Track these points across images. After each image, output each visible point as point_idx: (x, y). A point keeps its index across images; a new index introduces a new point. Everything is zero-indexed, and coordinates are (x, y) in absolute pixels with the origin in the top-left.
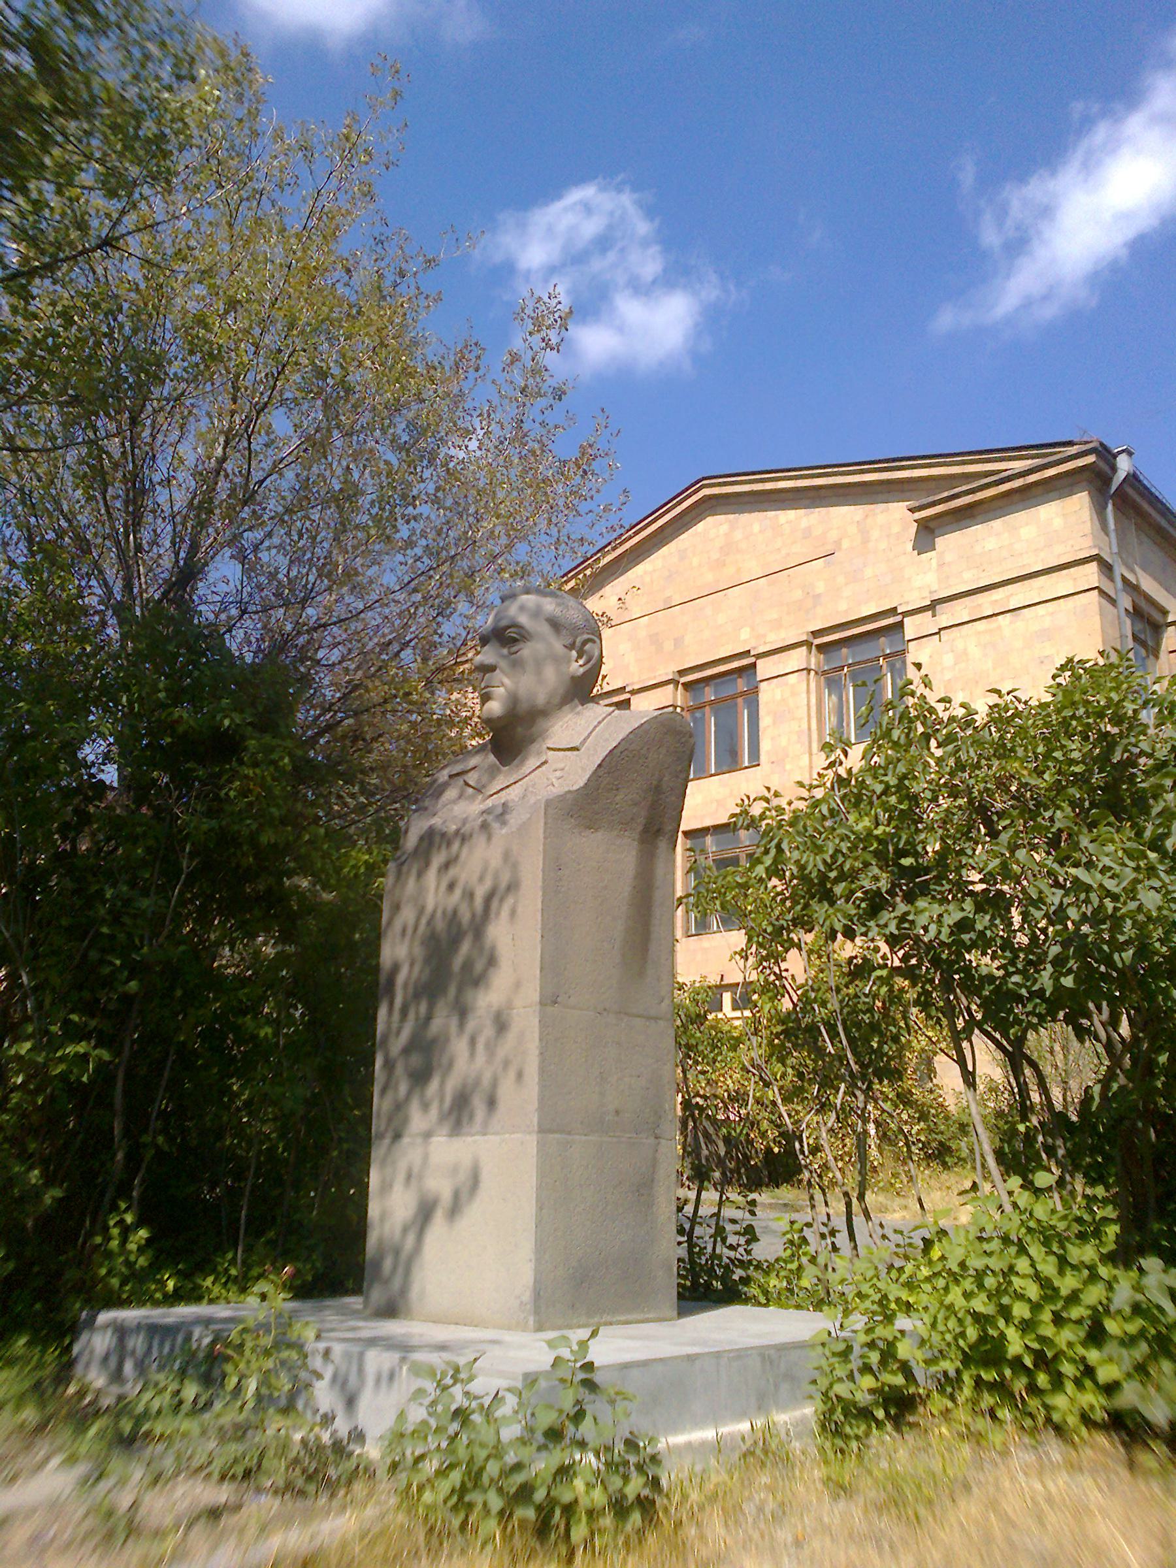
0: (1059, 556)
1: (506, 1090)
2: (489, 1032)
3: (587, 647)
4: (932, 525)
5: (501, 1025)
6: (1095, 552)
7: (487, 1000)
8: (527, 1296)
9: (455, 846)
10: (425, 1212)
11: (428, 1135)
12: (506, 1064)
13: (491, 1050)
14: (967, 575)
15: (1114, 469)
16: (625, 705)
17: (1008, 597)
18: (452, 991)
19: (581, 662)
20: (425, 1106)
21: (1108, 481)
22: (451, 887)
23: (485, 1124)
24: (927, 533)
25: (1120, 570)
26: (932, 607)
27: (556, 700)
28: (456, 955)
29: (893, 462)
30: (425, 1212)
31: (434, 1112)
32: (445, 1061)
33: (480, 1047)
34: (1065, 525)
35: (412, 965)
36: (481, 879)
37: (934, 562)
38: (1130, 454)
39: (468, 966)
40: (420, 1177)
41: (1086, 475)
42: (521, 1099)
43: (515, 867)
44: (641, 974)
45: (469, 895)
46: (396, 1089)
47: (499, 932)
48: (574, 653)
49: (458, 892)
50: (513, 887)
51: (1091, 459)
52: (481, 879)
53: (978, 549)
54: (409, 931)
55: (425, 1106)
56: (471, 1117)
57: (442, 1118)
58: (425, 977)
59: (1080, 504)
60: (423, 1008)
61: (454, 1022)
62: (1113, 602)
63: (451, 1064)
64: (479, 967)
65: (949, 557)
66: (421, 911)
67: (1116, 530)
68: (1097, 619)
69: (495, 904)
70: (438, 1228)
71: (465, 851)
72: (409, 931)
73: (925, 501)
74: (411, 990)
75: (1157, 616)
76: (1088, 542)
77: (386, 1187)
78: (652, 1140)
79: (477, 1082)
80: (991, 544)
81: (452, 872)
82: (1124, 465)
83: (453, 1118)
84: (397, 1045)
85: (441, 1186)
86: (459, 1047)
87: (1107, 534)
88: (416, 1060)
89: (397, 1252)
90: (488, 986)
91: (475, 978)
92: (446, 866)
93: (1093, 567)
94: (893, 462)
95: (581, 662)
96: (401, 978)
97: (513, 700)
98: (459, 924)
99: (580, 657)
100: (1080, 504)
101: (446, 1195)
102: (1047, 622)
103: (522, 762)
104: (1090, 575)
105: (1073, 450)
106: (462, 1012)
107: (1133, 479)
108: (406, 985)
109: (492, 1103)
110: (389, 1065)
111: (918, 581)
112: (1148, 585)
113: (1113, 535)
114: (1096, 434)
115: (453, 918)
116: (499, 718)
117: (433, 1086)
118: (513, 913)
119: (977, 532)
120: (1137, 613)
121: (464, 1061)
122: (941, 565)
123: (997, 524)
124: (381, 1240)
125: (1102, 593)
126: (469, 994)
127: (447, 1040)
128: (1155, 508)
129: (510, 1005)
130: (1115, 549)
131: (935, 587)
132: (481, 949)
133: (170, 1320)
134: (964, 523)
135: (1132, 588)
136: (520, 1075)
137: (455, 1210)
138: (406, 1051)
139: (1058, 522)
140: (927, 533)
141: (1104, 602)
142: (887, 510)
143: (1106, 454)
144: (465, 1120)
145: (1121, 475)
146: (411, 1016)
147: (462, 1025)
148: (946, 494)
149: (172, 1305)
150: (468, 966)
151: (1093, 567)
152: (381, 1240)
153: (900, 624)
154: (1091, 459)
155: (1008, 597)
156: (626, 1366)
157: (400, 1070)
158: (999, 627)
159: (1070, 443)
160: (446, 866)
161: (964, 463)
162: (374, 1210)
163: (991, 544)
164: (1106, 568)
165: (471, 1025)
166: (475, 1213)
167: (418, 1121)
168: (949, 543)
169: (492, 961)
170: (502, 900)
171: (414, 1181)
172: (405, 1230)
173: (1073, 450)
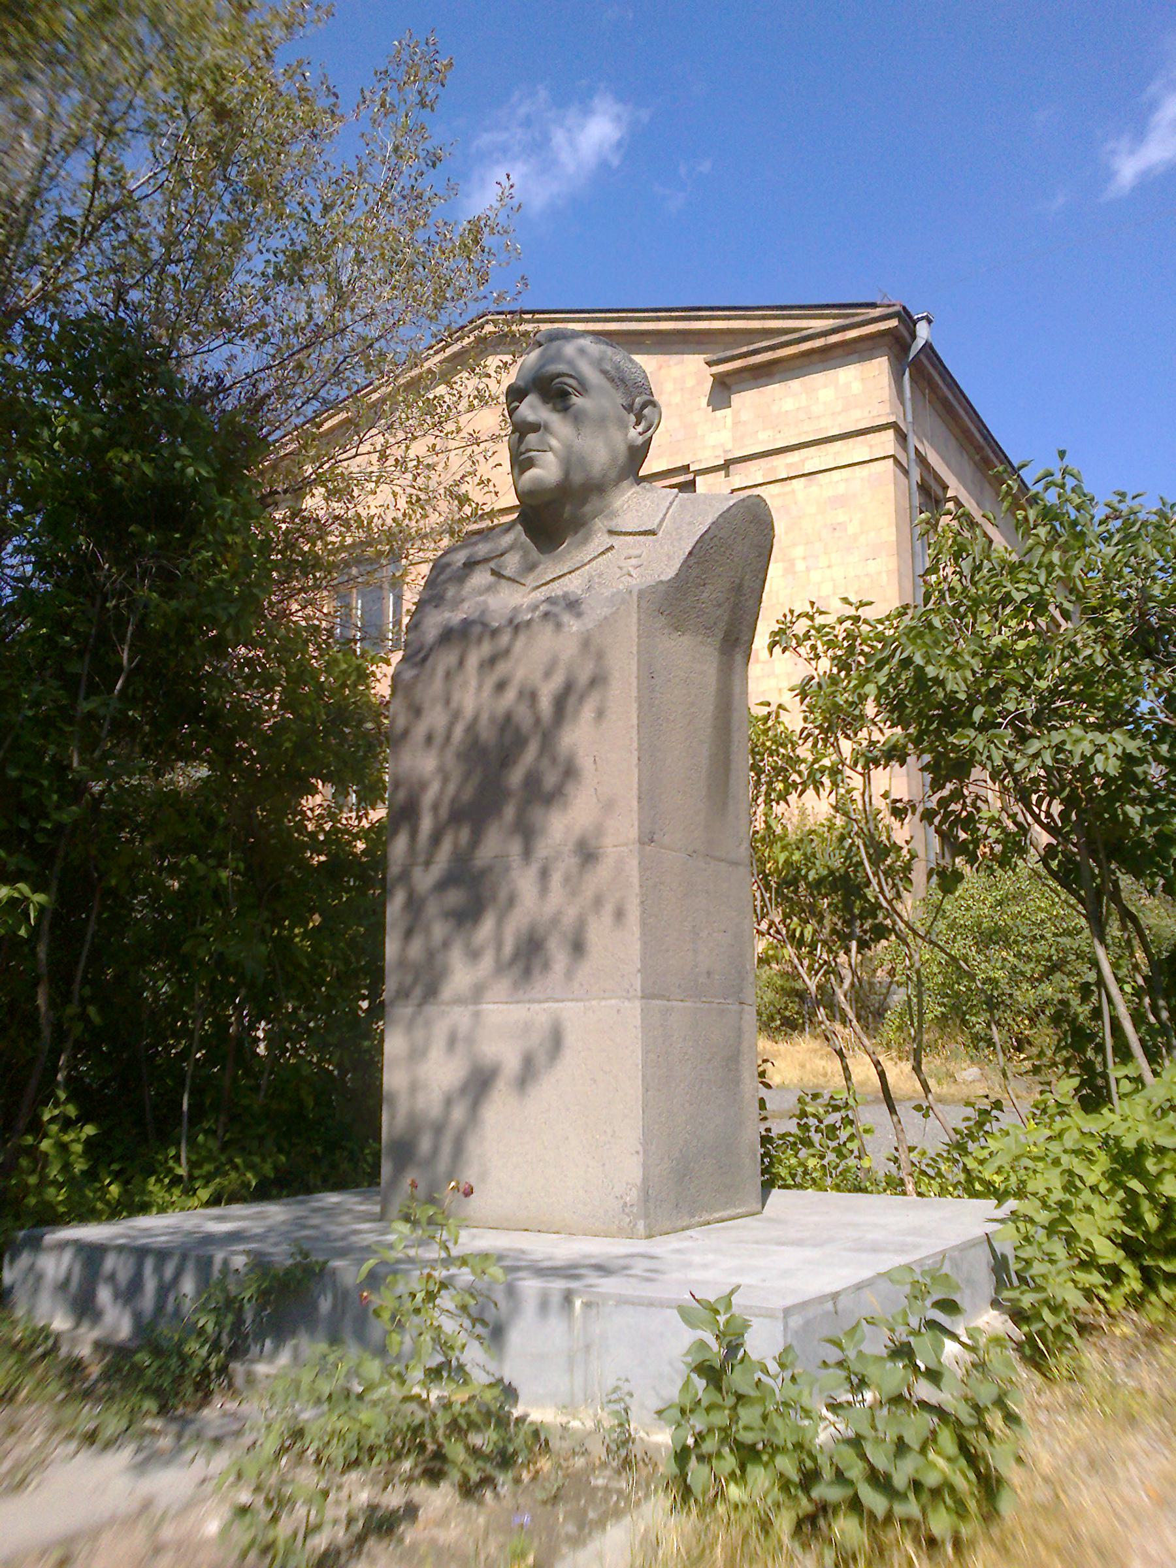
0: (857, 420)
1: (599, 932)
2: (568, 862)
3: (646, 411)
4: (727, 380)
5: (587, 853)
6: (892, 419)
7: (561, 827)
8: (633, 1196)
9: (505, 639)
10: (480, 1083)
11: (477, 993)
12: (598, 902)
13: (572, 885)
14: (762, 436)
15: (914, 336)
16: (690, 486)
17: (803, 461)
18: (509, 812)
19: (640, 429)
20: (474, 955)
21: (906, 348)
22: (501, 686)
23: (569, 975)
24: (723, 390)
25: (913, 441)
26: (726, 466)
27: (613, 474)
28: (508, 775)
29: (693, 311)
30: (480, 1083)
31: (487, 962)
32: (503, 895)
33: (556, 878)
34: (864, 389)
35: (445, 780)
36: (548, 674)
37: (729, 421)
38: (930, 322)
39: (532, 781)
40: (470, 1040)
41: (887, 339)
42: (617, 948)
43: (600, 656)
44: (725, 804)
45: (530, 696)
46: (428, 932)
47: (579, 737)
48: (633, 418)
49: (510, 695)
50: (598, 681)
51: (894, 323)
52: (548, 674)
53: (775, 409)
54: (438, 740)
55: (474, 955)
56: (546, 966)
57: (500, 968)
58: (467, 795)
59: (879, 369)
60: (465, 834)
61: (515, 848)
62: (906, 472)
63: (512, 901)
64: (550, 780)
65: (744, 416)
66: (456, 716)
67: (913, 398)
68: (892, 487)
69: (572, 700)
70: (499, 1109)
71: (519, 645)
72: (438, 740)
73: (722, 355)
74: (444, 812)
75: (939, 492)
76: (886, 408)
77: (417, 1054)
78: (735, 1007)
79: (555, 921)
80: (789, 404)
81: (502, 668)
82: (923, 332)
83: (521, 965)
84: (424, 880)
85: (507, 1056)
86: (525, 882)
87: (903, 403)
88: (455, 897)
89: (439, 1129)
90: (565, 806)
91: (543, 794)
92: (491, 661)
93: (890, 433)
94: (693, 311)
95: (640, 429)
96: (428, 798)
97: (568, 462)
98: (517, 730)
99: (638, 423)
100: (879, 369)
101: (511, 1063)
102: (841, 489)
103: (586, 540)
104: (886, 442)
105: (876, 312)
106: (527, 833)
107: (928, 346)
108: (435, 807)
109: (578, 947)
110: (414, 905)
111: (713, 439)
112: (934, 459)
113: (908, 404)
114: (899, 299)
115: (507, 722)
116: (551, 490)
117: (486, 927)
118: (600, 714)
119: (774, 390)
120: (923, 488)
121: (530, 898)
122: (736, 424)
123: (795, 384)
124: (412, 1116)
125: (897, 462)
126: (537, 813)
127: (507, 869)
128: (944, 380)
129: (599, 830)
130: (910, 419)
131: (729, 446)
132: (554, 761)
133: (237, 1209)
134: (763, 380)
135: (922, 460)
136: (619, 914)
137: (528, 1074)
138: (442, 886)
139: (856, 387)
140: (723, 390)
141: (898, 471)
142: (682, 362)
143: (907, 320)
144: (536, 972)
145: (920, 343)
146: (446, 847)
147: (527, 853)
148: (745, 349)
149: (639, 699)
150: (532, 781)
151: (890, 433)
152: (412, 1116)
153: (693, 483)
154: (894, 323)
155: (803, 461)
156: (859, 1287)
157: (432, 908)
158: (793, 491)
159: (873, 305)
160: (491, 661)
161: (763, 318)
162: (393, 1079)
163: (789, 404)
164: (902, 437)
165: (542, 849)
166: (551, 1088)
167: (461, 976)
168: (745, 401)
169: (570, 772)
170: (582, 699)
171: (460, 1047)
172: (448, 1102)
173: (876, 312)
